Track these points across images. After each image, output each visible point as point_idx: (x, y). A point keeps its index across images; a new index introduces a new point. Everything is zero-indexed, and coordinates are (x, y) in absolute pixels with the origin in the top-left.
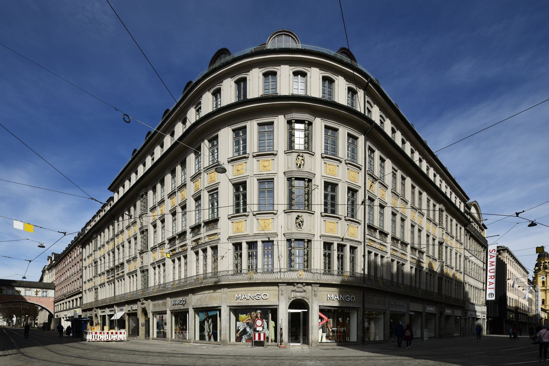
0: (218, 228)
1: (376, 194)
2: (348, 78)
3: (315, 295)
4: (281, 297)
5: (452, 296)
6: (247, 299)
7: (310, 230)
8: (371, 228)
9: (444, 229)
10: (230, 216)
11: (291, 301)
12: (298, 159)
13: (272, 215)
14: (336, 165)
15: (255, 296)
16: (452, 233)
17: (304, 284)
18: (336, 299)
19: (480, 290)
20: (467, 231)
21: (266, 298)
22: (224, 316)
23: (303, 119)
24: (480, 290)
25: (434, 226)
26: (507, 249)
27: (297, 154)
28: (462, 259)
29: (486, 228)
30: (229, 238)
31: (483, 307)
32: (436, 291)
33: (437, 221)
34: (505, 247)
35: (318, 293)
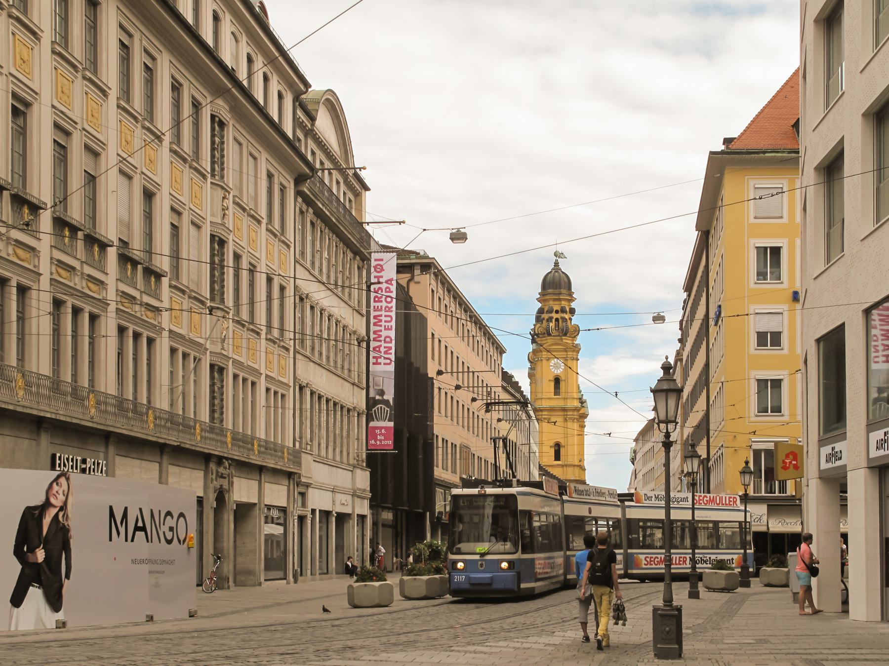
5: (287, 444)
9: (227, 191)
16: (198, 158)
25: (197, 178)
26: (433, 263)
28: (289, 302)
31: (358, 472)
33: (206, 164)
34: (428, 257)
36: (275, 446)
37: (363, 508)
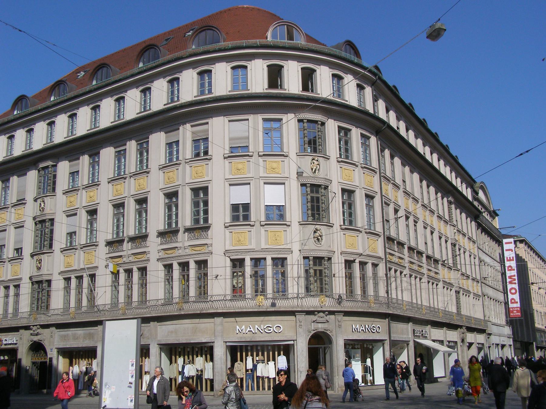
0: (209, 238)
1: (390, 197)
2: (355, 74)
3: (340, 326)
4: (300, 330)
6: (253, 332)
7: (330, 246)
8: (390, 239)
10: (228, 224)
11: (311, 334)
12: (313, 163)
13: (285, 226)
14: (352, 170)
15: (265, 329)
17: (327, 313)
18: (362, 330)
19: (501, 303)
20: (479, 226)
21: (279, 332)
22: (218, 355)
23: (316, 119)
24: (501, 303)
27: (311, 158)
29: (497, 215)
30: (226, 252)
32: (454, 310)
33: (447, 217)
35: (343, 323)
36: (417, 305)
37: (511, 342)
